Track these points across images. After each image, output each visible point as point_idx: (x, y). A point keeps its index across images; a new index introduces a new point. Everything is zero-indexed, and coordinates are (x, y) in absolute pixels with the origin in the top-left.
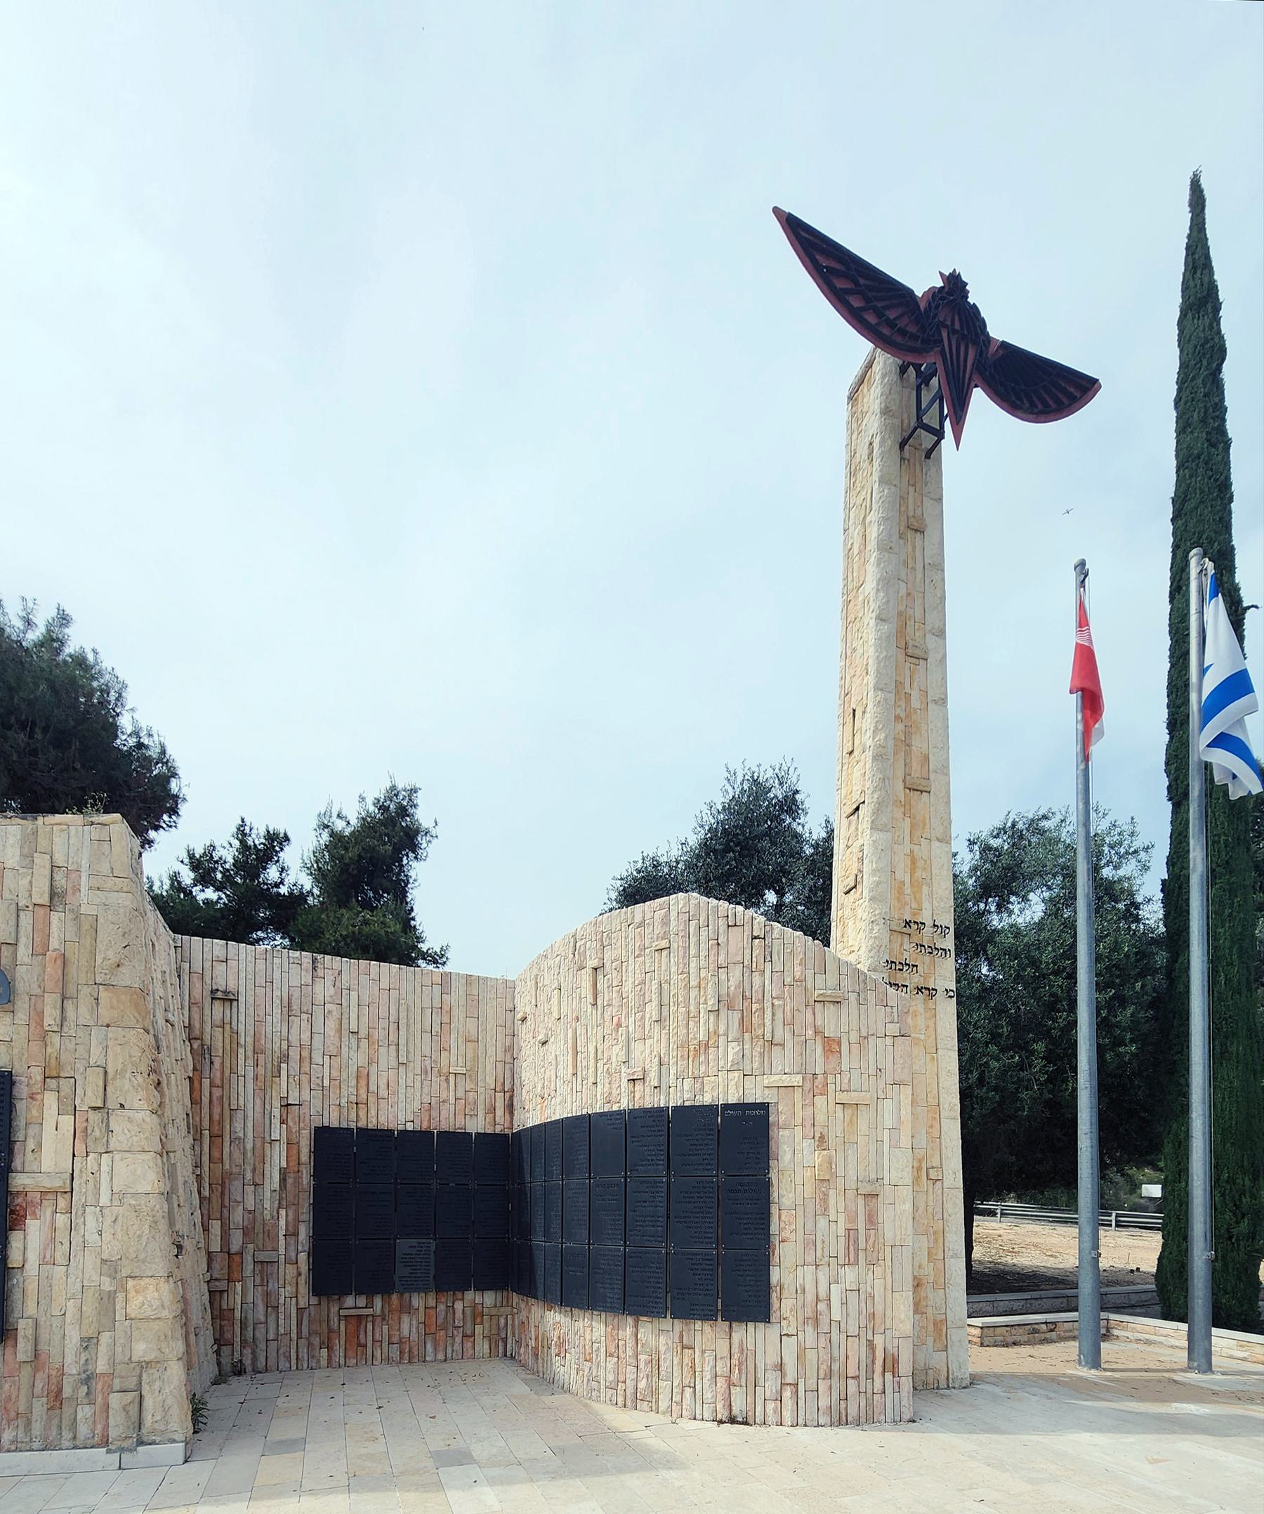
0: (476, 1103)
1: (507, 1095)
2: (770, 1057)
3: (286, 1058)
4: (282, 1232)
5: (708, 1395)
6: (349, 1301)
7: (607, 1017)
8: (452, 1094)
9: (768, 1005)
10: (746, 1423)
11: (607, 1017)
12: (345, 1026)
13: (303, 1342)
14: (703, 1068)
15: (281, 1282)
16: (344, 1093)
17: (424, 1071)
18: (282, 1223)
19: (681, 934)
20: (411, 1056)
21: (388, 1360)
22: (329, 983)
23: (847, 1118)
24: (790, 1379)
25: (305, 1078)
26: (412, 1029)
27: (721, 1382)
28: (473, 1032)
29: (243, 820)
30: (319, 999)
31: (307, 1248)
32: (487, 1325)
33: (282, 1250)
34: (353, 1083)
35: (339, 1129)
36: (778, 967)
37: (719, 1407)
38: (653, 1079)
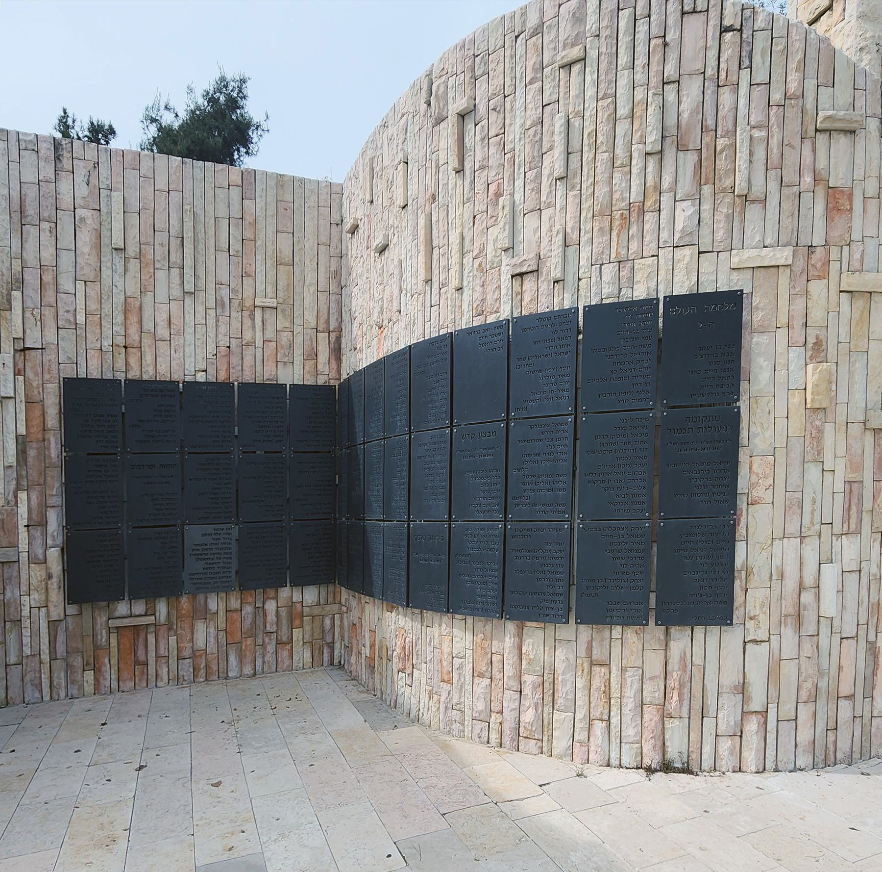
0: (291, 346)
1: (333, 336)
2: (743, 221)
3: (20, 283)
4: (23, 521)
5: (630, 732)
6: (122, 608)
7: (480, 186)
8: (259, 334)
9: (741, 136)
10: (686, 770)
11: (480, 186)
12: (105, 240)
13: (58, 664)
14: (634, 246)
15: (24, 588)
16: (107, 332)
17: (219, 304)
18: (23, 510)
19: (603, 34)
20: (201, 284)
21: (178, 680)
22: (80, 178)
23: (856, 315)
24: (756, 704)
25: (48, 313)
26: (201, 246)
27: (651, 715)
28: (286, 252)
29: (65, 112)
30: (66, 201)
31: (59, 541)
32: (307, 628)
33: (23, 545)
34: (120, 318)
35: (101, 383)
36: (761, 76)
37: (647, 748)
38: (553, 268)
